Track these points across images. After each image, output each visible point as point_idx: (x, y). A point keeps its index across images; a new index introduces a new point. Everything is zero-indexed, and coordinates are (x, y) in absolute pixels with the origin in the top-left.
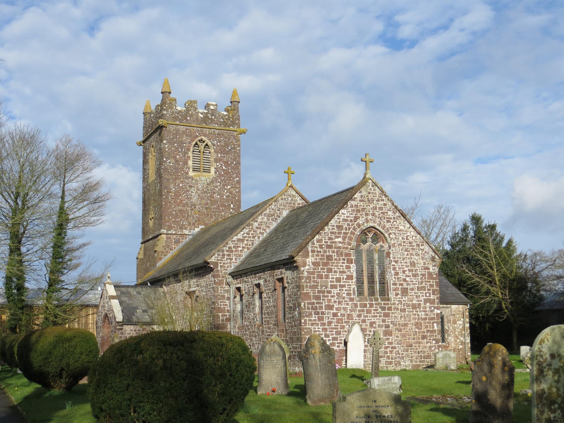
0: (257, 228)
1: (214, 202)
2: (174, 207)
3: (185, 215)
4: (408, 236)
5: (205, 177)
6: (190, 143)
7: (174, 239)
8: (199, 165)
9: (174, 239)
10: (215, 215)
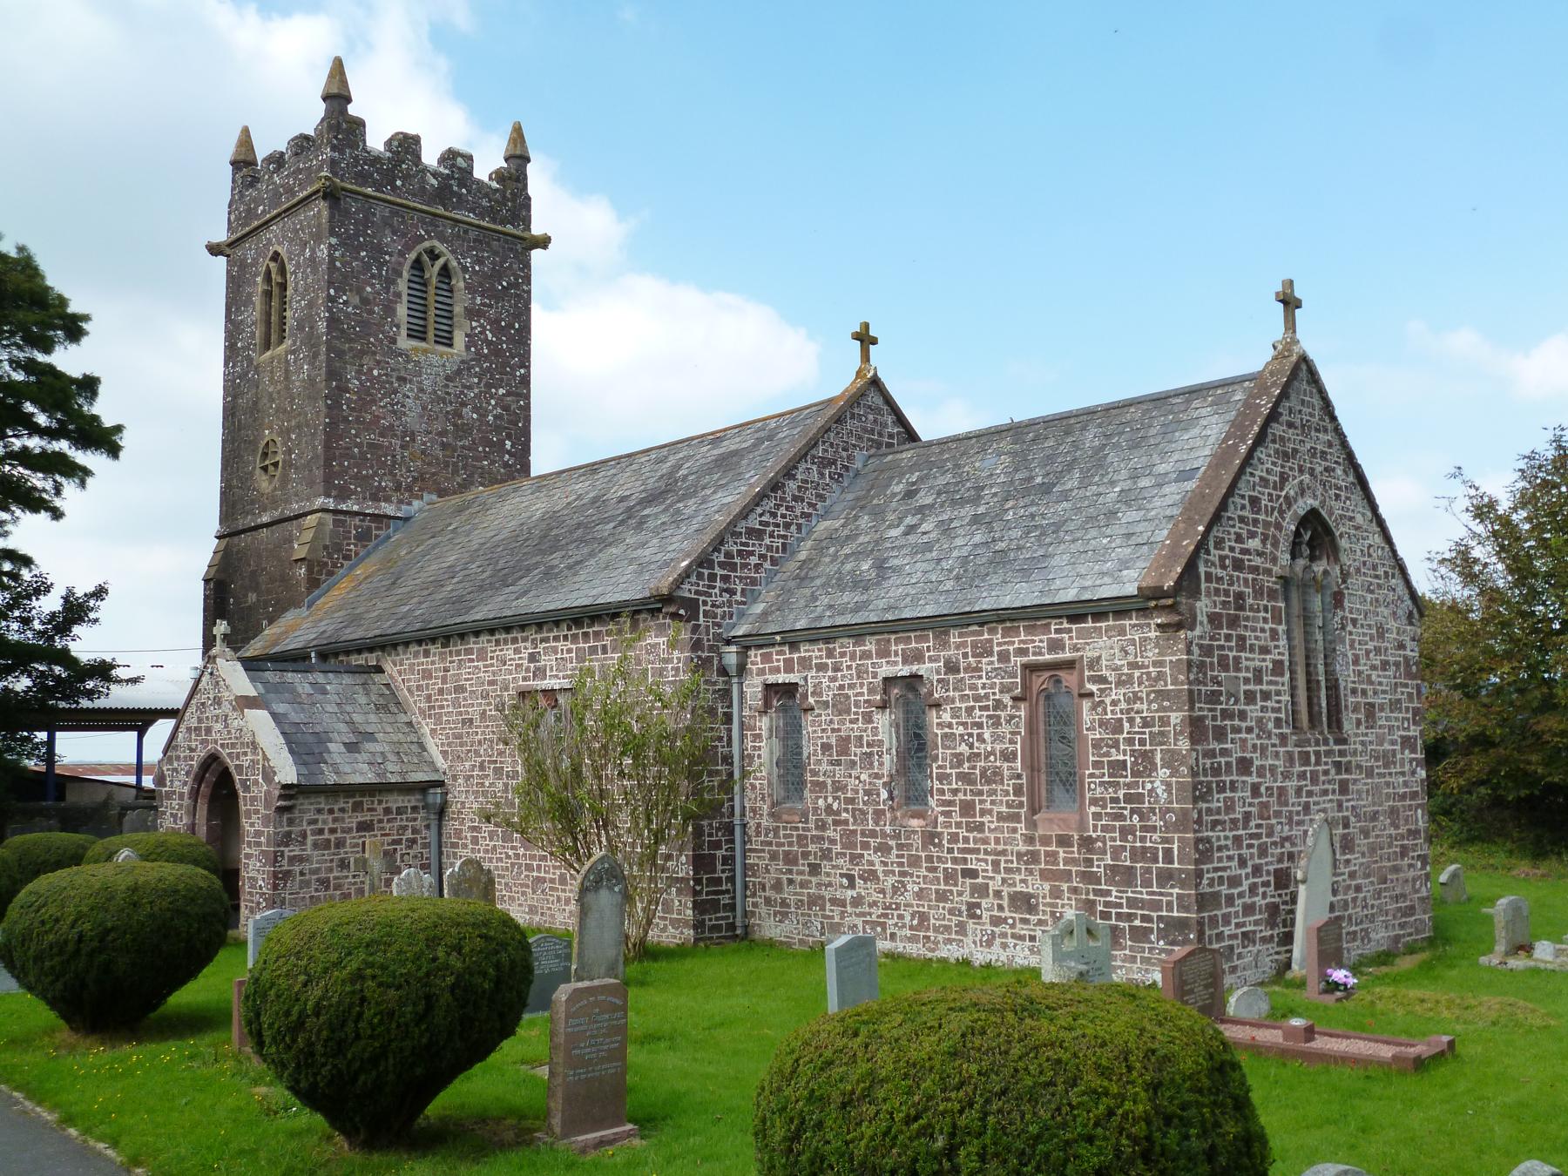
0: (795, 498)
1: (462, 430)
2: (356, 436)
3: (386, 461)
4: (1370, 546)
5: (442, 357)
6: (402, 254)
7: (356, 528)
8: (421, 322)
9: (356, 528)
10: (464, 467)
